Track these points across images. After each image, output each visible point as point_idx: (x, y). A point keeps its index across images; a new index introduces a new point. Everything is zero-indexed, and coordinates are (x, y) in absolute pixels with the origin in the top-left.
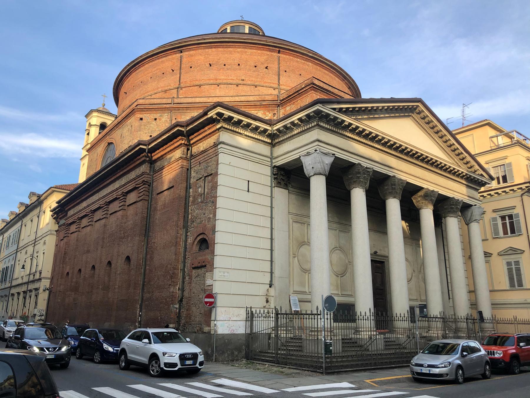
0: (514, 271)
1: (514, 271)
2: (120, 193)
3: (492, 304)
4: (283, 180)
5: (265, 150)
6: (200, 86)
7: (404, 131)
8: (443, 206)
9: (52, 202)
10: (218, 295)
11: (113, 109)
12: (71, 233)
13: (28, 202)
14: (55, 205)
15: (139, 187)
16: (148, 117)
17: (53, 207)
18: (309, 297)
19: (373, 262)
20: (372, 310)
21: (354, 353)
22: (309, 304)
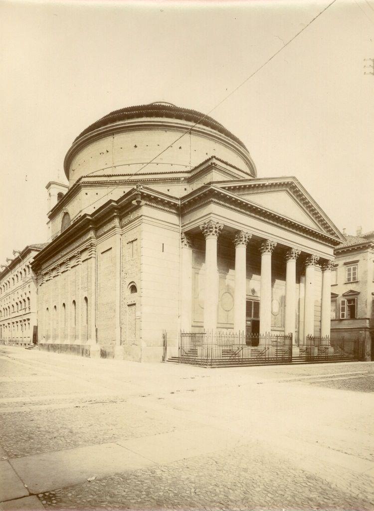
0: (252, 314)
1: (252, 314)
2: (76, 252)
3: (233, 328)
4: (188, 243)
5: (174, 219)
6: (129, 165)
7: (280, 203)
8: (303, 260)
9: (30, 258)
10: (349, 318)
11: (66, 183)
12: (72, 267)
13: (13, 258)
14: (32, 260)
15: (88, 248)
16: (91, 191)
17: (31, 262)
18: (231, 326)
19: (249, 304)
20: (245, 334)
21: (228, 358)
22: (202, 328)
